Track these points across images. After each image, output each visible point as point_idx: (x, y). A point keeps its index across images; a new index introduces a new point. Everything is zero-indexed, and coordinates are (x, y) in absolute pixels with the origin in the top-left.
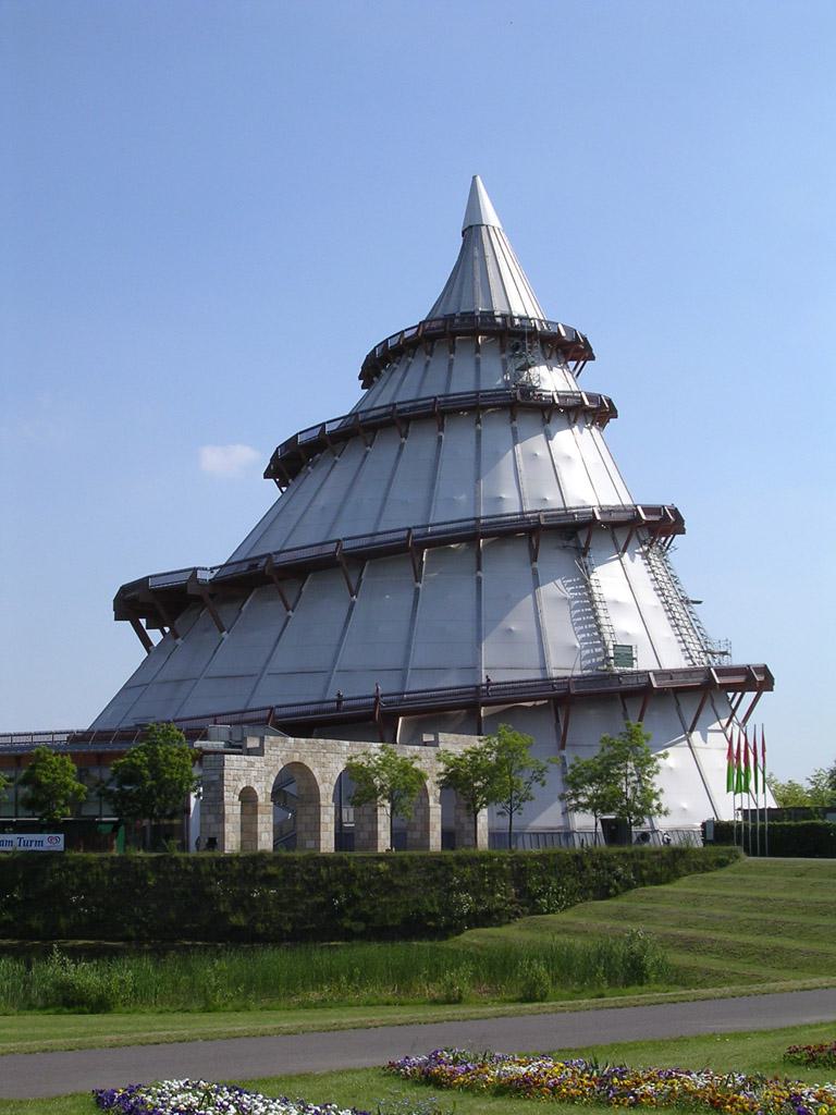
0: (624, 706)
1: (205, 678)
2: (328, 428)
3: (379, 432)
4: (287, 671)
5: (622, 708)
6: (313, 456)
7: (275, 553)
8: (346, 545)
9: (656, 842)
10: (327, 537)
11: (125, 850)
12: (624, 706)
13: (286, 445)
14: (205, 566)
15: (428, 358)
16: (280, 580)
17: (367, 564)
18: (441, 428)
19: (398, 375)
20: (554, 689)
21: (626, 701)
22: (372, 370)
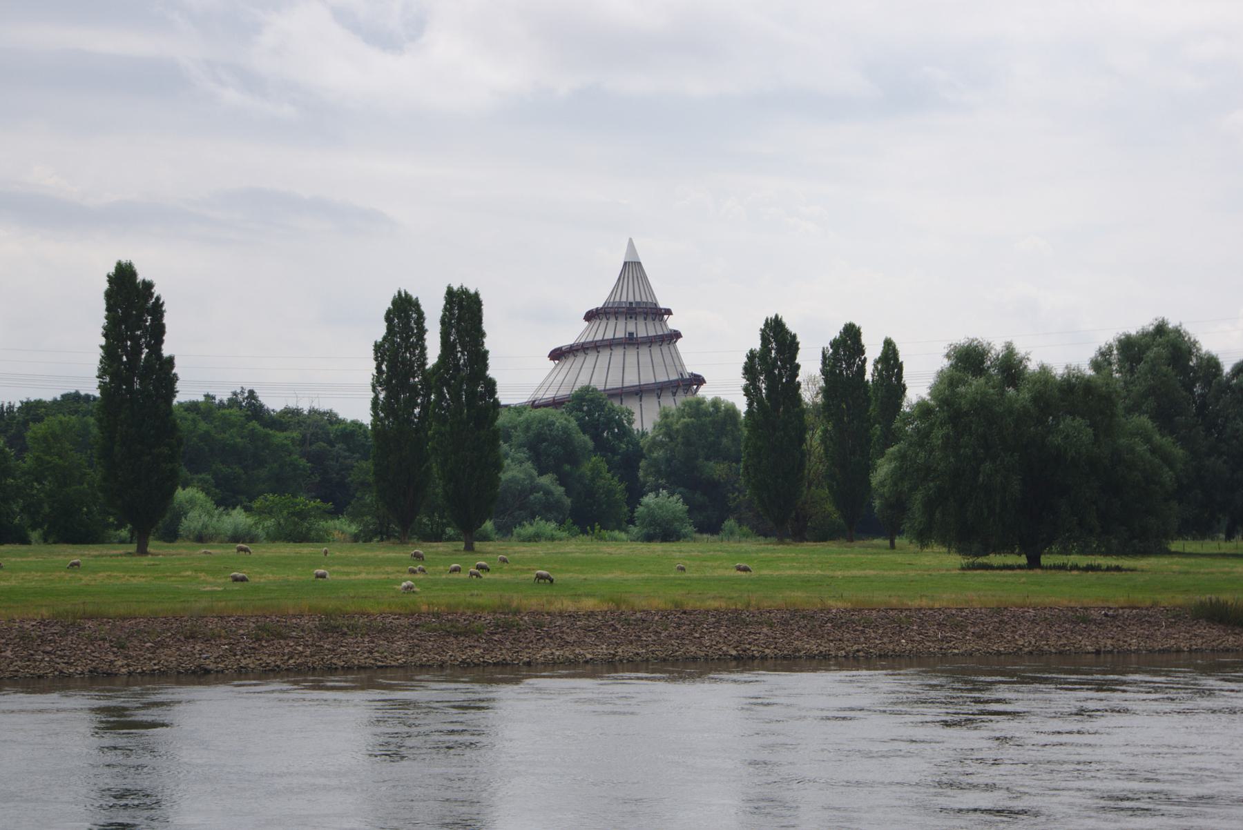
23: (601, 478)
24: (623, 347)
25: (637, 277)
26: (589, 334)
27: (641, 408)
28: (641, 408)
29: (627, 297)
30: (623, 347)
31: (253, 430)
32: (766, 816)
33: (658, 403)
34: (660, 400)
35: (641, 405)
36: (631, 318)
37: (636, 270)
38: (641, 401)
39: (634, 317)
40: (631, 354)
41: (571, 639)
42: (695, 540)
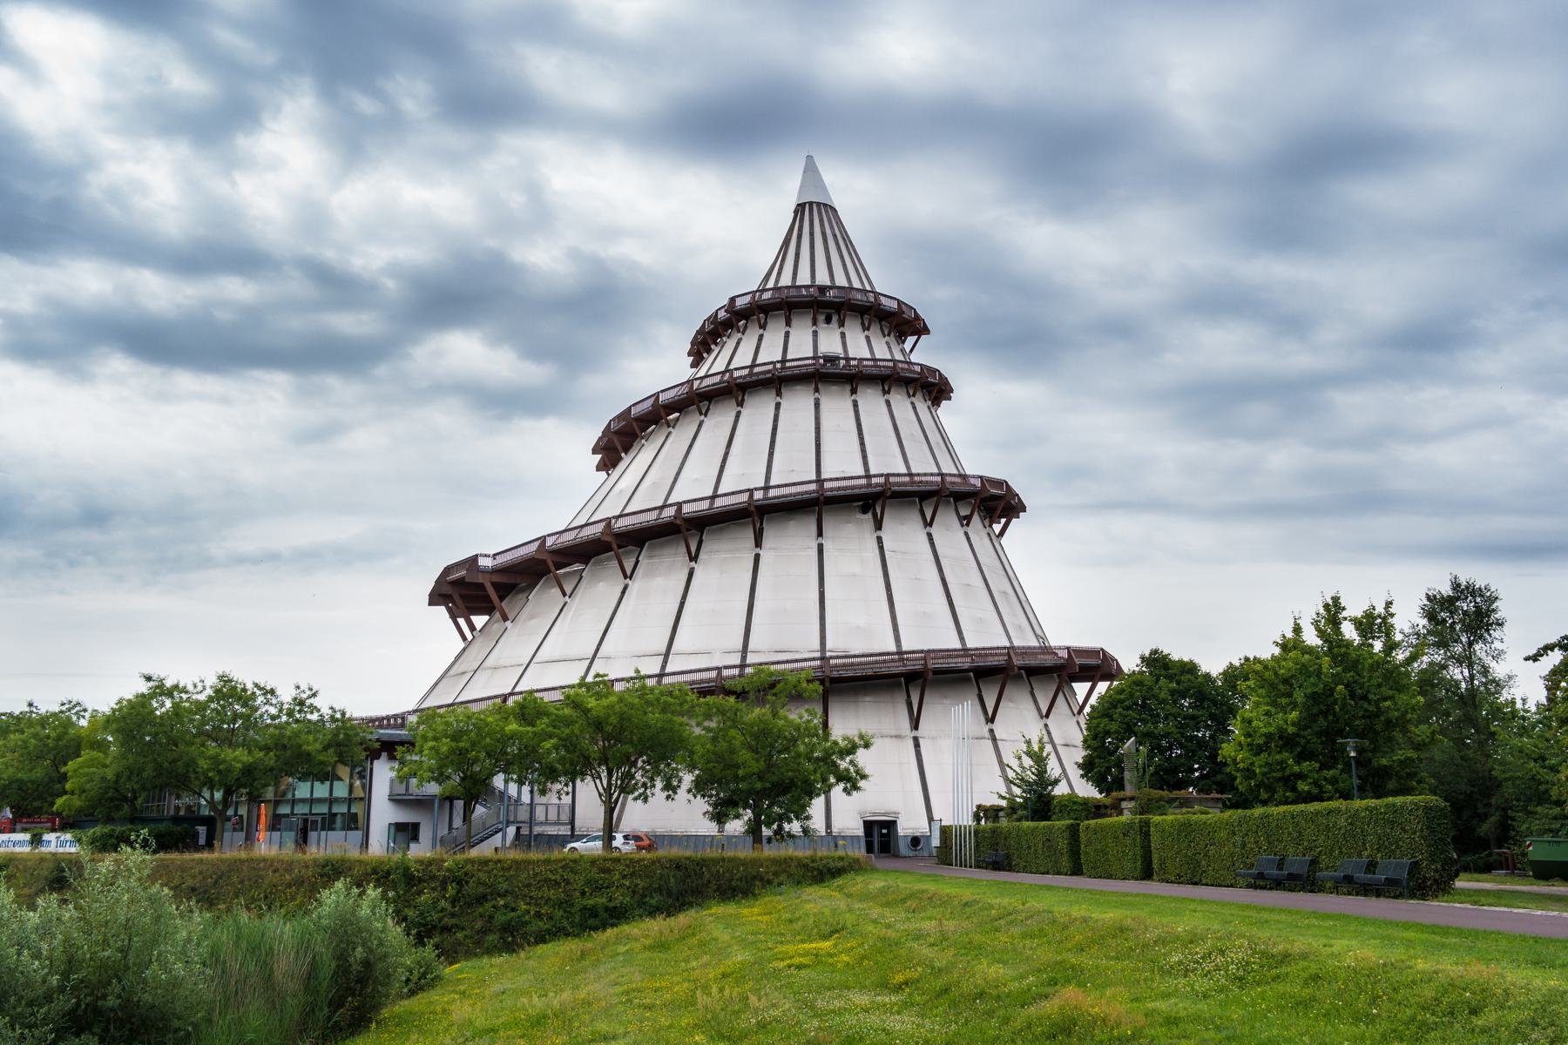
0: (1030, 682)
1: (522, 665)
2: (662, 398)
3: (713, 402)
4: (653, 653)
5: (977, 690)
6: (644, 430)
7: (614, 517)
8: (686, 509)
9: (5, 806)
10: (623, 510)
11: (729, 946)
12: (1030, 682)
13: (619, 417)
14: (487, 553)
15: (761, 331)
16: (620, 547)
17: (647, 544)
18: (779, 394)
19: (730, 345)
20: (905, 666)
21: (1031, 678)
22: (702, 346)
23: (1326, 792)
24: (848, 388)
25: (835, 236)
26: (715, 359)
27: (881, 548)
28: (881, 548)
29: (805, 275)
30: (848, 388)
31: (1141, 822)
32: (201, 1040)
33: (925, 539)
34: (934, 530)
35: (879, 540)
36: (828, 320)
37: (821, 221)
38: (758, 544)
39: (835, 318)
40: (837, 406)
41: (147, 959)
42: (874, 870)
